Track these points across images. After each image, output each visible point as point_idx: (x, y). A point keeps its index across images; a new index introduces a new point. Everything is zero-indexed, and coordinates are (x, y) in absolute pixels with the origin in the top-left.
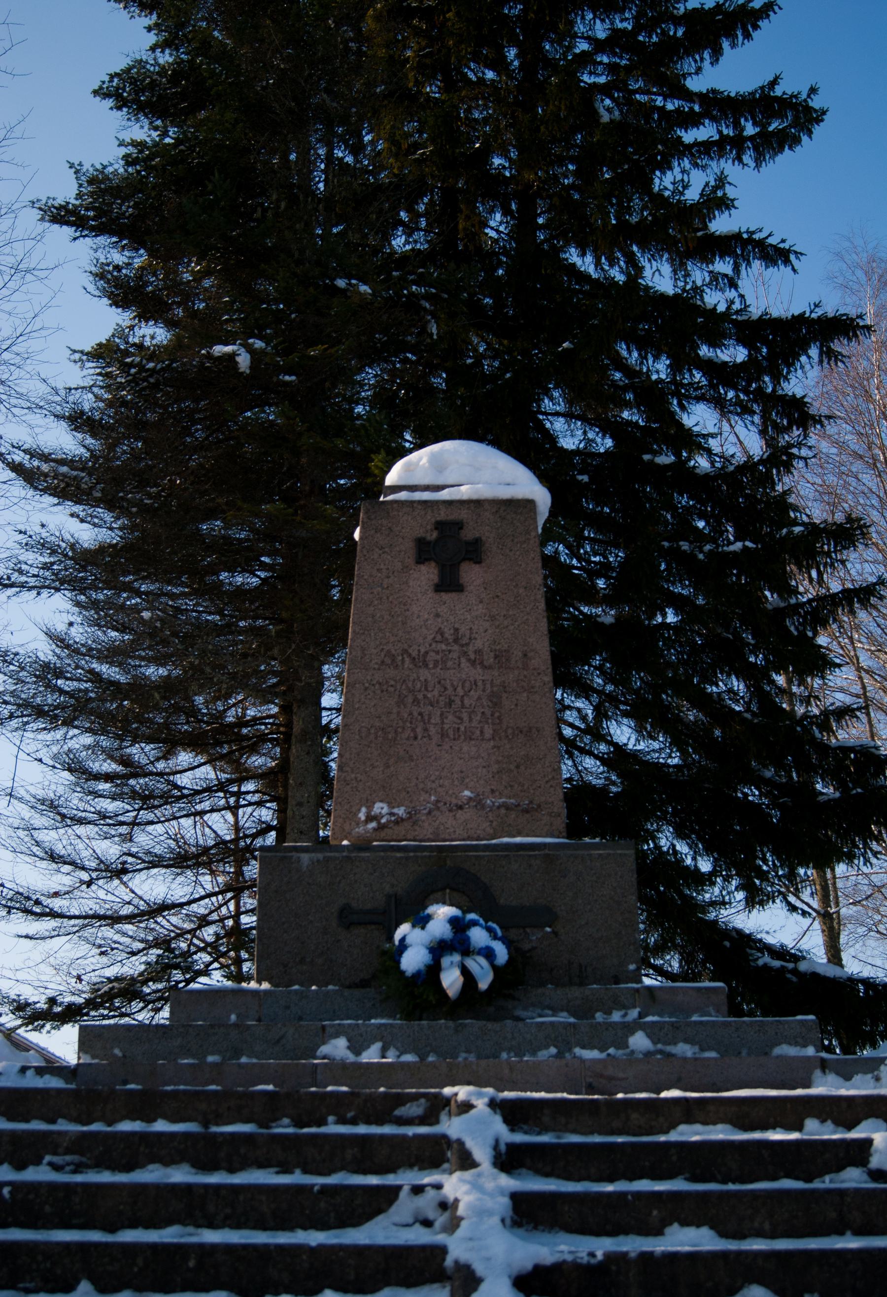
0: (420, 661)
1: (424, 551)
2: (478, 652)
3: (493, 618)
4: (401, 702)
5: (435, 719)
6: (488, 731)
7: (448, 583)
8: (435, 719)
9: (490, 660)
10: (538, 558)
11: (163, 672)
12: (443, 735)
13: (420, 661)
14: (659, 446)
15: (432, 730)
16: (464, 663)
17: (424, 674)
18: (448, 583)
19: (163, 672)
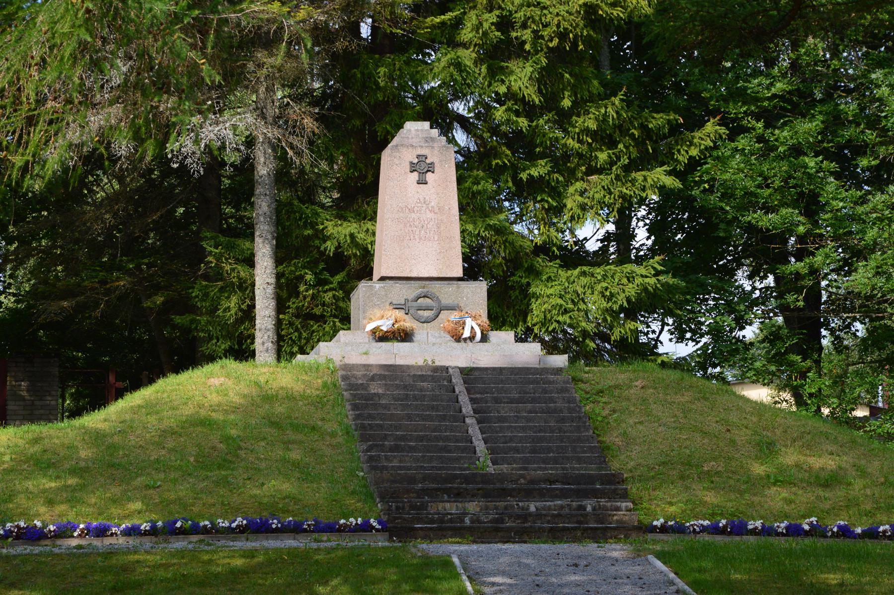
0: (412, 211)
1: (413, 168)
2: (432, 207)
3: (438, 194)
4: (405, 226)
5: (417, 233)
6: (436, 238)
7: (422, 182)
8: (417, 233)
9: (436, 210)
10: (172, 519)
11: (159, 214)
12: (420, 239)
13: (412, 211)
14: (194, 173)
15: (416, 237)
16: (428, 212)
17: (413, 215)
18: (422, 182)
19: (159, 214)
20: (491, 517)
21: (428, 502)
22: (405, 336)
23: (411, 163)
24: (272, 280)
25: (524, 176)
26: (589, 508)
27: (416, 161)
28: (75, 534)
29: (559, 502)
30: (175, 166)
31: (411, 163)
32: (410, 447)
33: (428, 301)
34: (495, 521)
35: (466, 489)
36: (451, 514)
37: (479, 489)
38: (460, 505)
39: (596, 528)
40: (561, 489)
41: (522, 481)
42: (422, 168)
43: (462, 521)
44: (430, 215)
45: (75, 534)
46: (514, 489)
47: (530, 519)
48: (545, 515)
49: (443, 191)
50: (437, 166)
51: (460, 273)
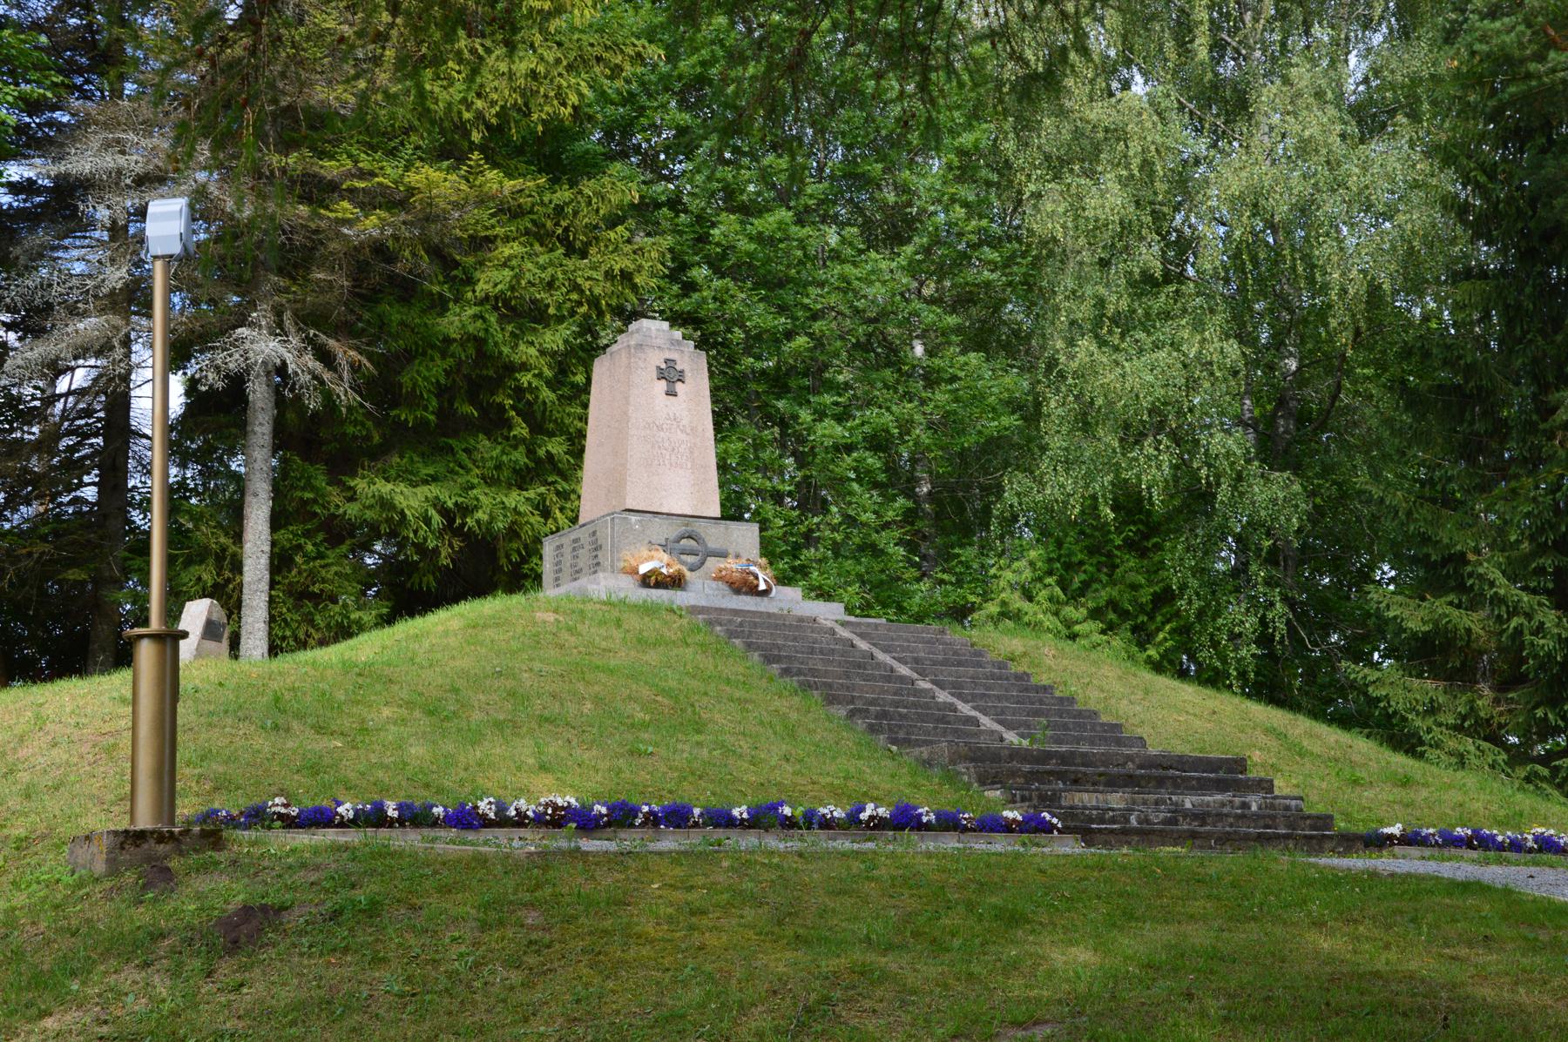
1: (662, 375)
7: (671, 393)
18: (671, 393)
20: (1162, 815)
21: (1062, 791)
22: (676, 582)
23: (659, 368)
24: (267, 548)
25: (541, 452)
26: (1254, 808)
27: (663, 366)
28: (638, 821)
29: (1219, 797)
30: (204, 389)
31: (659, 368)
32: (900, 714)
33: (692, 543)
34: (1166, 822)
35: (1085, 774)
36: (1113, 810)
37: (1101, 775)
38: (1100, 796)
39: (1311, 837)
40: (1199, 779)
41: (1130, 765)
42: (670, 376)
43: (1127, 821)
44: (683, 436)
45: (638, 821)
46: (1142, 776)
47: (1209, 820)
48: (1227, 815)
49: (690, 408)
50: (688, 374)
51: (717, 513)
